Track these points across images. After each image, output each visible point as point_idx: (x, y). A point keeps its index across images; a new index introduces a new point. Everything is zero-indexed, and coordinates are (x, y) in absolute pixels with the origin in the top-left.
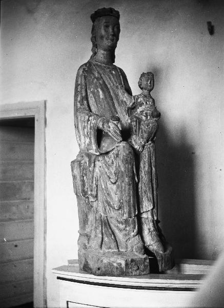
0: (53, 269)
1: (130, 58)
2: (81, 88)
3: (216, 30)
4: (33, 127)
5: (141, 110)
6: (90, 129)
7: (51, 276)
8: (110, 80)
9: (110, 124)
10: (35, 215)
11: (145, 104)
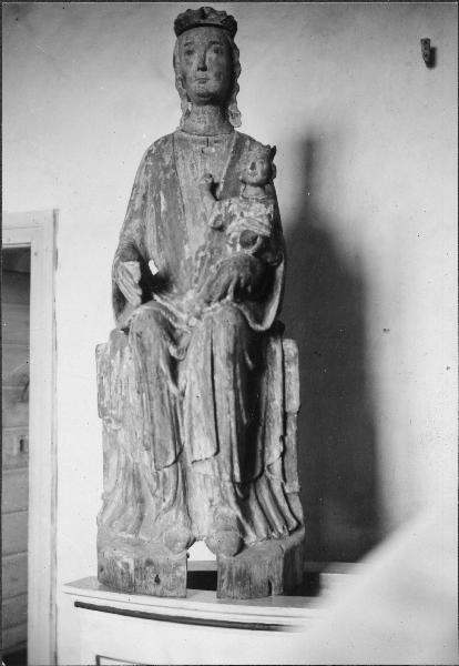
0: (66, 585)
1: (261, 113)
3: (440, 58)
4: (27, 275)
7: (65, 603)
10: (30, 469)
11: (238, 217)
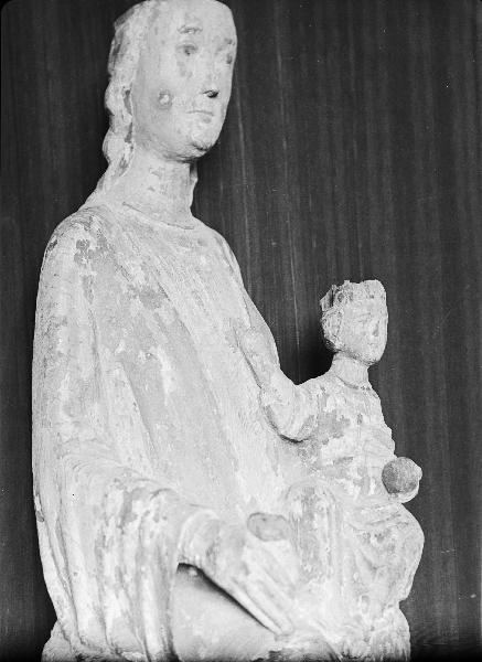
2: (74, 342)
5: (340, 452)
6: (140, 557)
8: (200, 303)
9: (247, 555)
11: (353, 421)
